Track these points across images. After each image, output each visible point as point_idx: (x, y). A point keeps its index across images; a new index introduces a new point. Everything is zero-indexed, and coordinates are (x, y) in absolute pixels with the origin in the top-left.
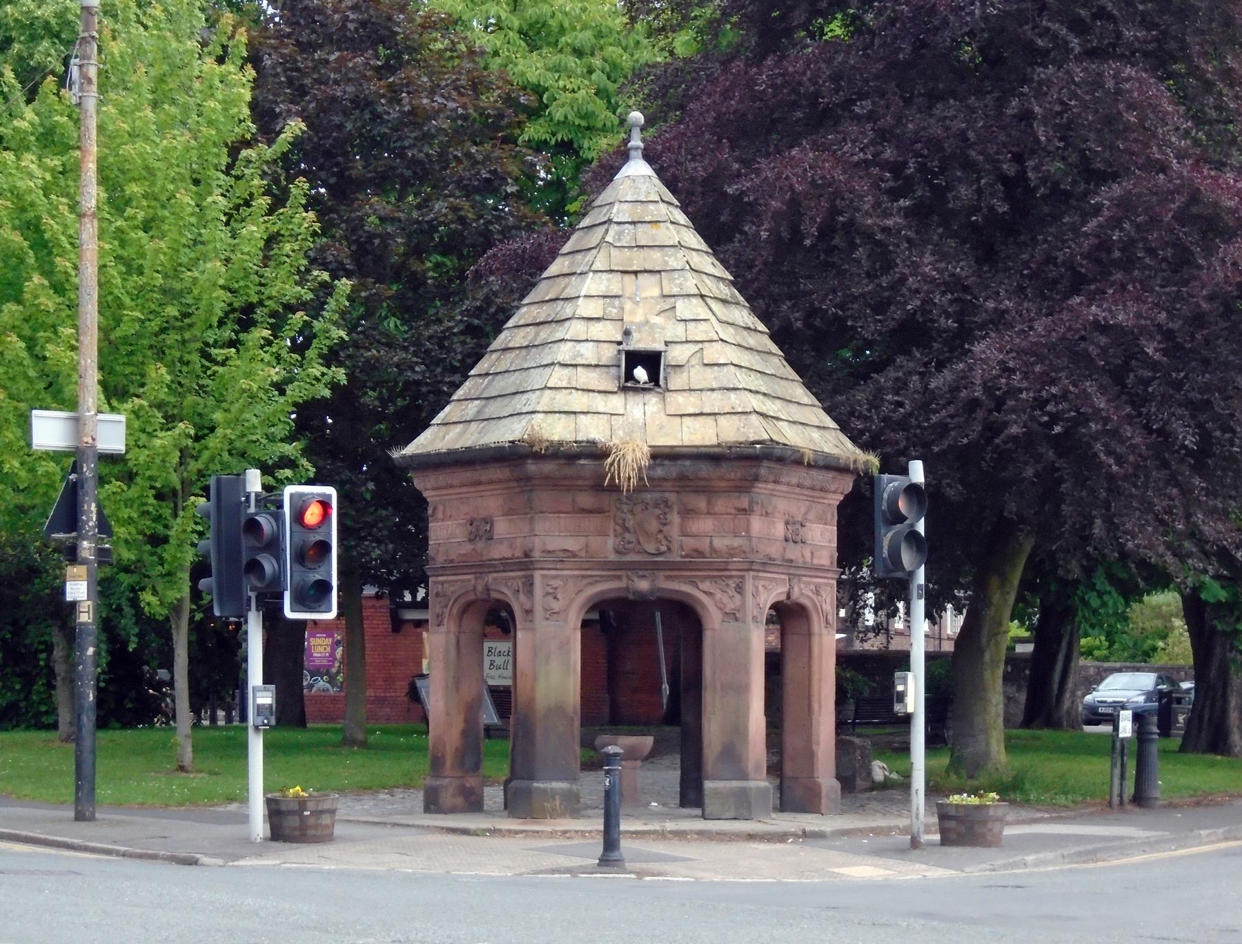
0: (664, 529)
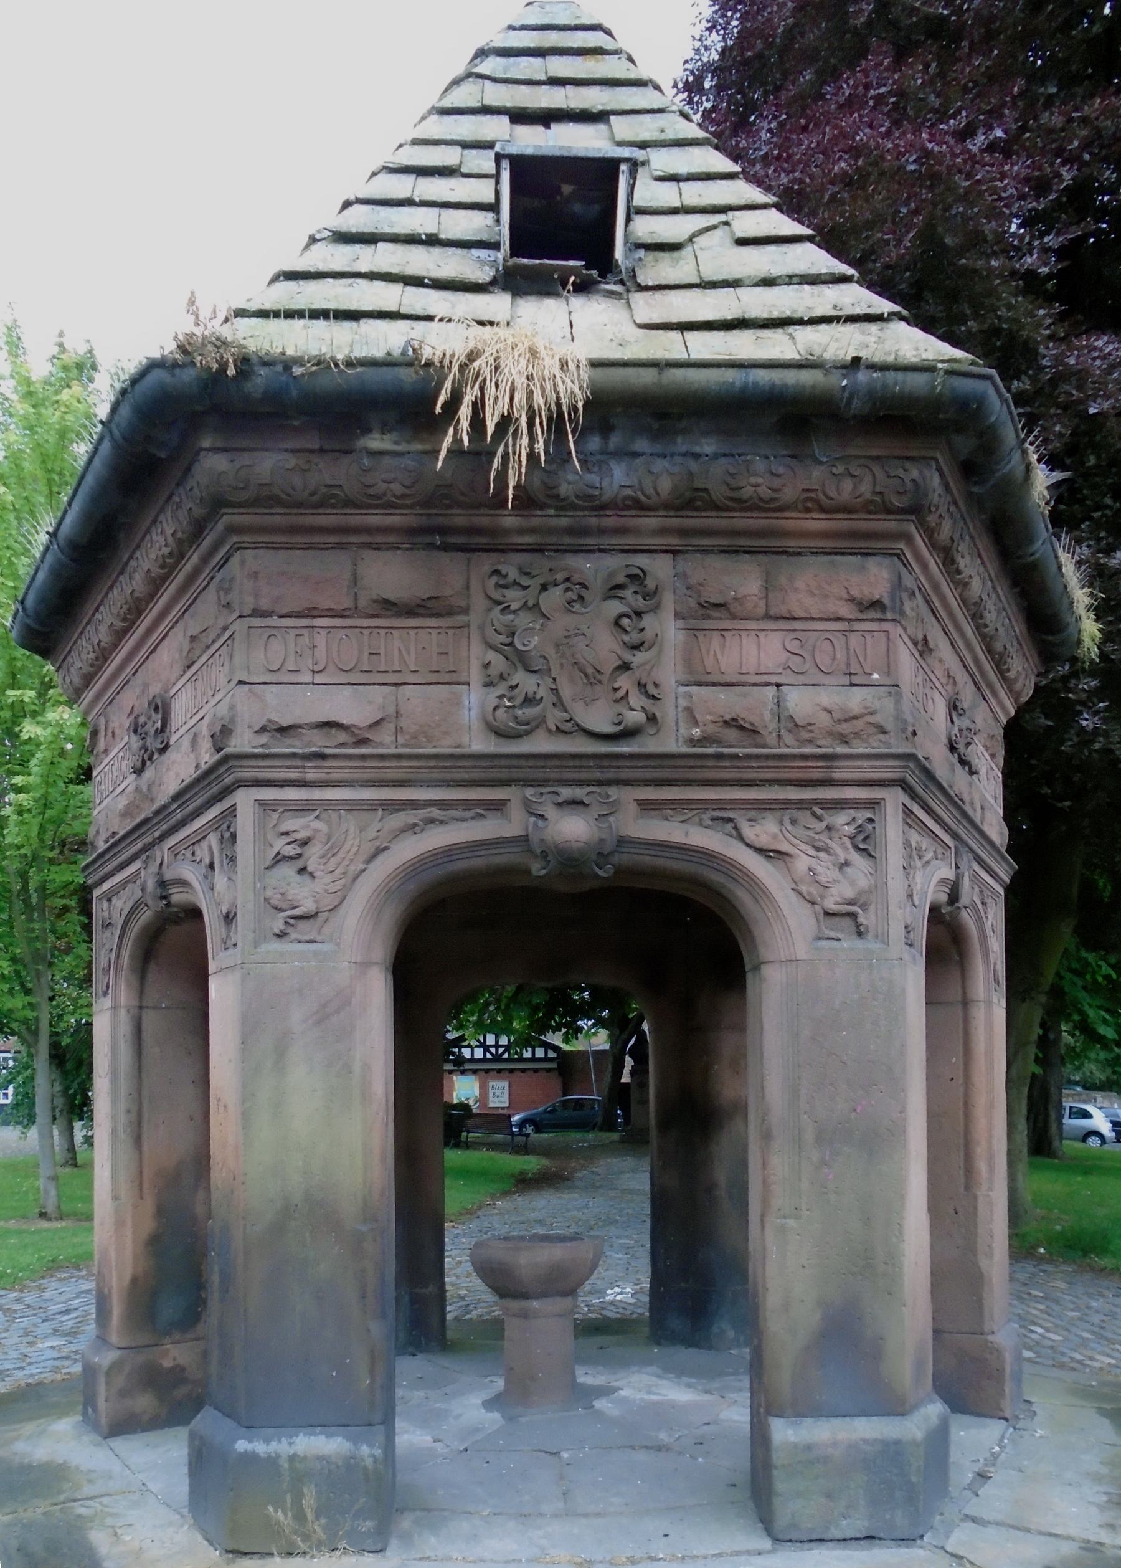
0: (638, 658)
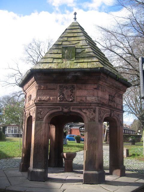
0: (73, 94)
